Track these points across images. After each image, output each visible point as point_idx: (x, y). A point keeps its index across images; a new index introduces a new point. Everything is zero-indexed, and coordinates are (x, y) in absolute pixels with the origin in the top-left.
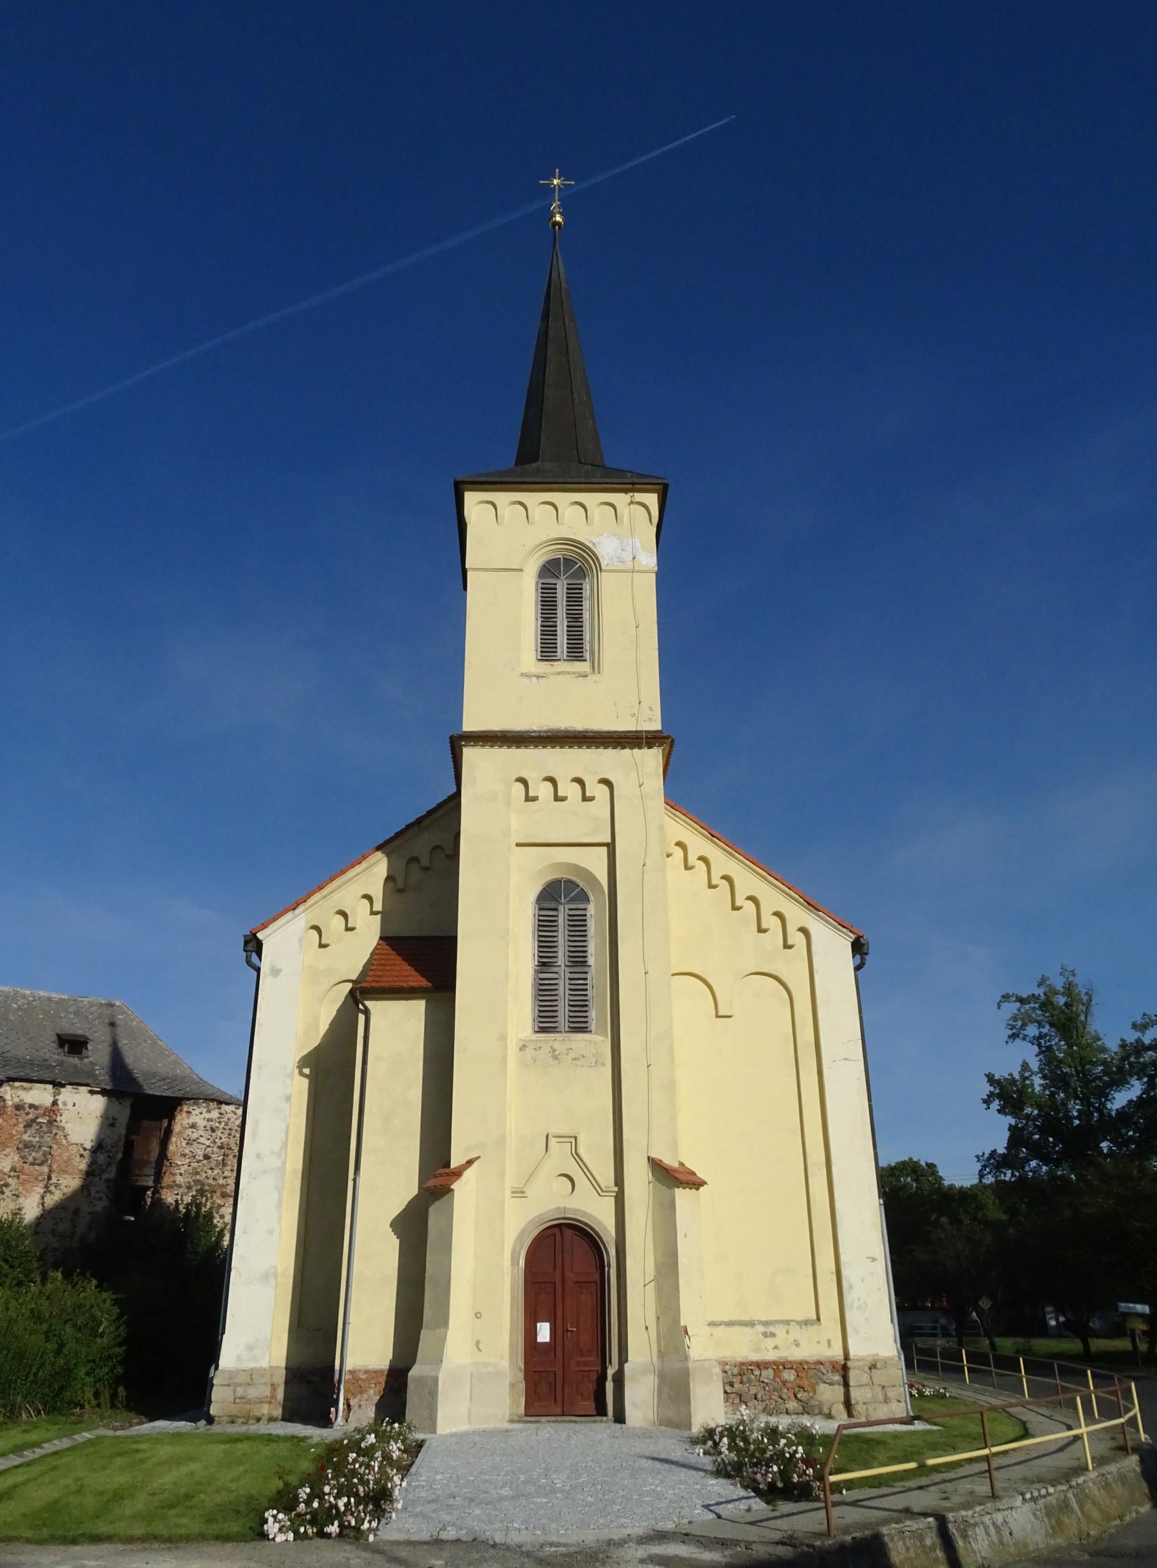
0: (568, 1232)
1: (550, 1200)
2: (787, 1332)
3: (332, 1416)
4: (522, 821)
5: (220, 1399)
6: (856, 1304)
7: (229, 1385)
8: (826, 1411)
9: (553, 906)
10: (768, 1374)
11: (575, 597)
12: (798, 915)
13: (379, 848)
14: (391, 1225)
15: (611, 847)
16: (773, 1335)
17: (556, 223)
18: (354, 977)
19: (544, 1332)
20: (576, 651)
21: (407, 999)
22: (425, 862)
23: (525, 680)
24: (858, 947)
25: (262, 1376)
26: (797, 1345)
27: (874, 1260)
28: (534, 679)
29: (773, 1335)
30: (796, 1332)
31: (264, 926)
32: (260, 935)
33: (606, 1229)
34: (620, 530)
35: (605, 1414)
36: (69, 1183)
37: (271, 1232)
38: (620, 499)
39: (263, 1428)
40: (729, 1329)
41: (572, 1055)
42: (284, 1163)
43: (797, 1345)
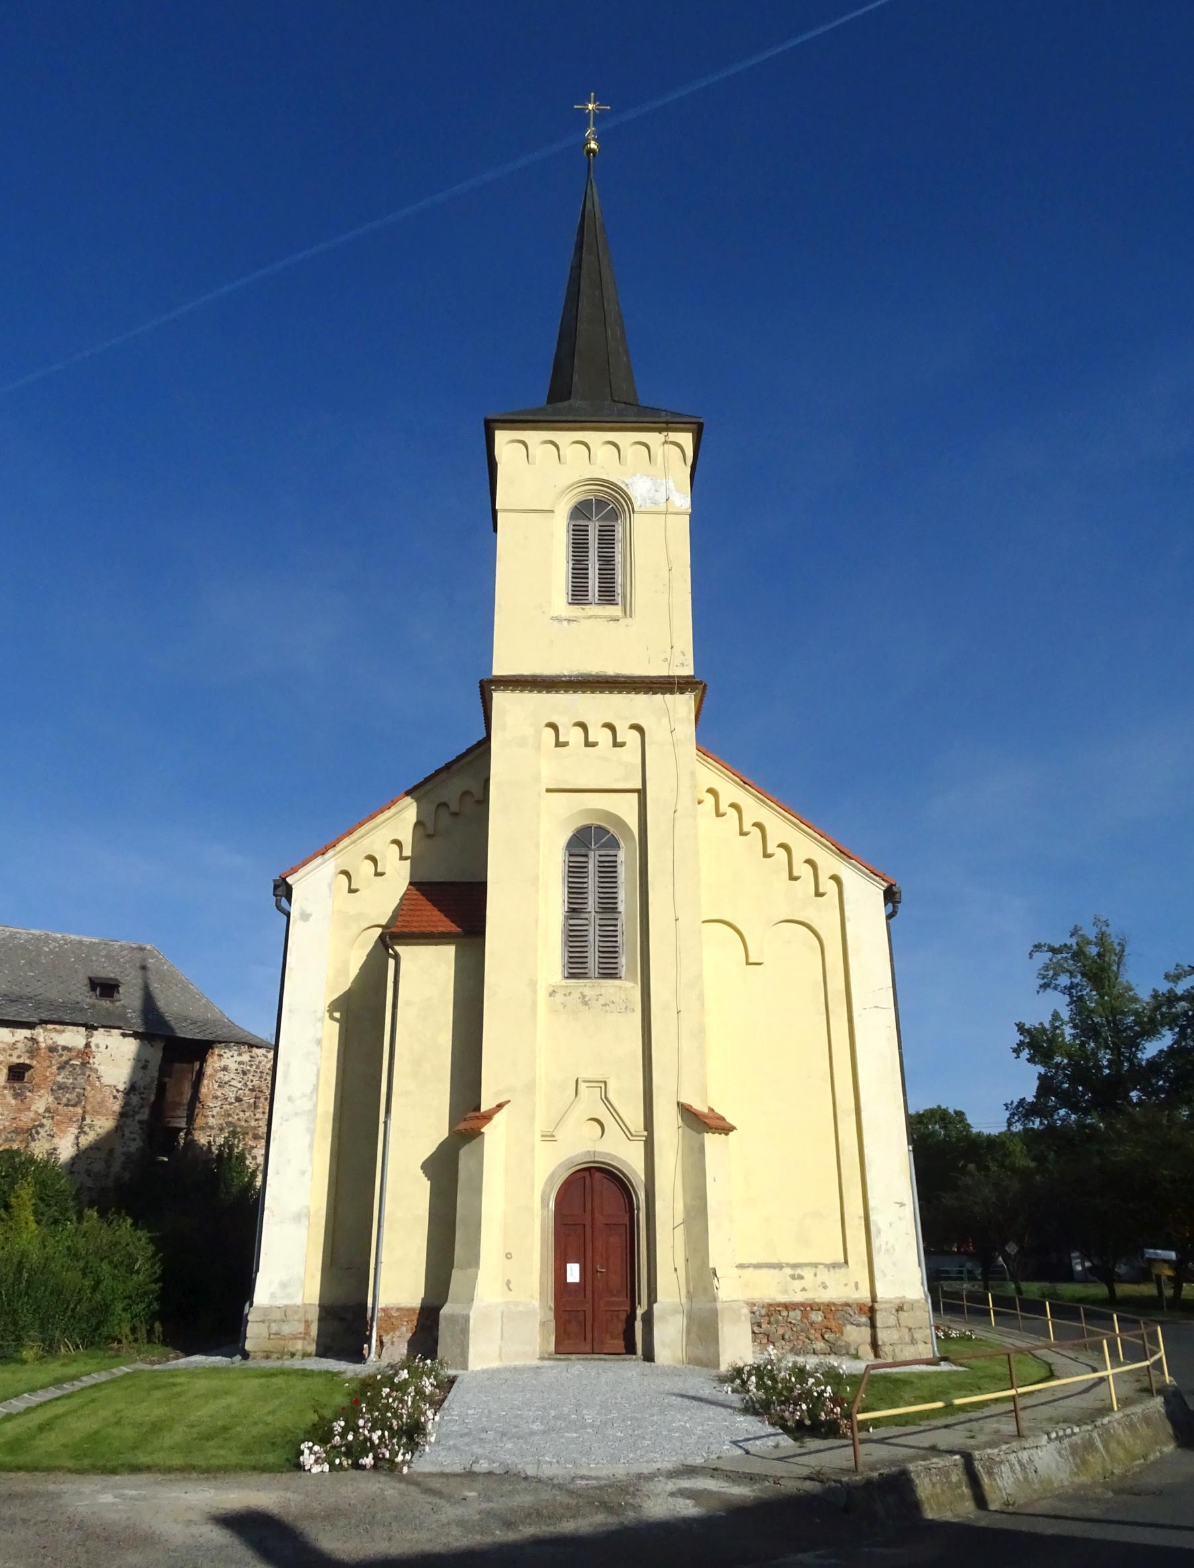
0: (598, 1175)
1: (579, 1143)
2: (815, 1275)
3: (365, 1352)
4: (555, 768)
5: (255, 1334)
6: (884, 1247)
7: (263, 1321)
8: (853, 1351)
9: (583, 852)
10: (795, 1316)
11: (607, 539)
12: (829, 862)
13: (408, 793)
14: (422, 1167)
15: (642, 793)
16: (801, 1277)
17: (591, 151)
18: (384, 923)
19: (573, 1273)
20: (608, 595)
21: (437, 944)
22: (454, 807)
23: (556, 623)
24: (890, 895)
25: (296, 1312)
26: (825, 1287)
27: (902, 1205)
28: (565, 623)
29: (801, 1277)
30: (824, 1275)
31: (294, 871)
32: (289, 880)
33: (635, 1172)
34: (654, 472)
35: (634, 1353)
36: (103, 1124)
37: (303, 1173)
38: (653, 438)
39: (298, 1363)
41: (602, 1001)
42: (315, 1105)
43: (825, 1287)
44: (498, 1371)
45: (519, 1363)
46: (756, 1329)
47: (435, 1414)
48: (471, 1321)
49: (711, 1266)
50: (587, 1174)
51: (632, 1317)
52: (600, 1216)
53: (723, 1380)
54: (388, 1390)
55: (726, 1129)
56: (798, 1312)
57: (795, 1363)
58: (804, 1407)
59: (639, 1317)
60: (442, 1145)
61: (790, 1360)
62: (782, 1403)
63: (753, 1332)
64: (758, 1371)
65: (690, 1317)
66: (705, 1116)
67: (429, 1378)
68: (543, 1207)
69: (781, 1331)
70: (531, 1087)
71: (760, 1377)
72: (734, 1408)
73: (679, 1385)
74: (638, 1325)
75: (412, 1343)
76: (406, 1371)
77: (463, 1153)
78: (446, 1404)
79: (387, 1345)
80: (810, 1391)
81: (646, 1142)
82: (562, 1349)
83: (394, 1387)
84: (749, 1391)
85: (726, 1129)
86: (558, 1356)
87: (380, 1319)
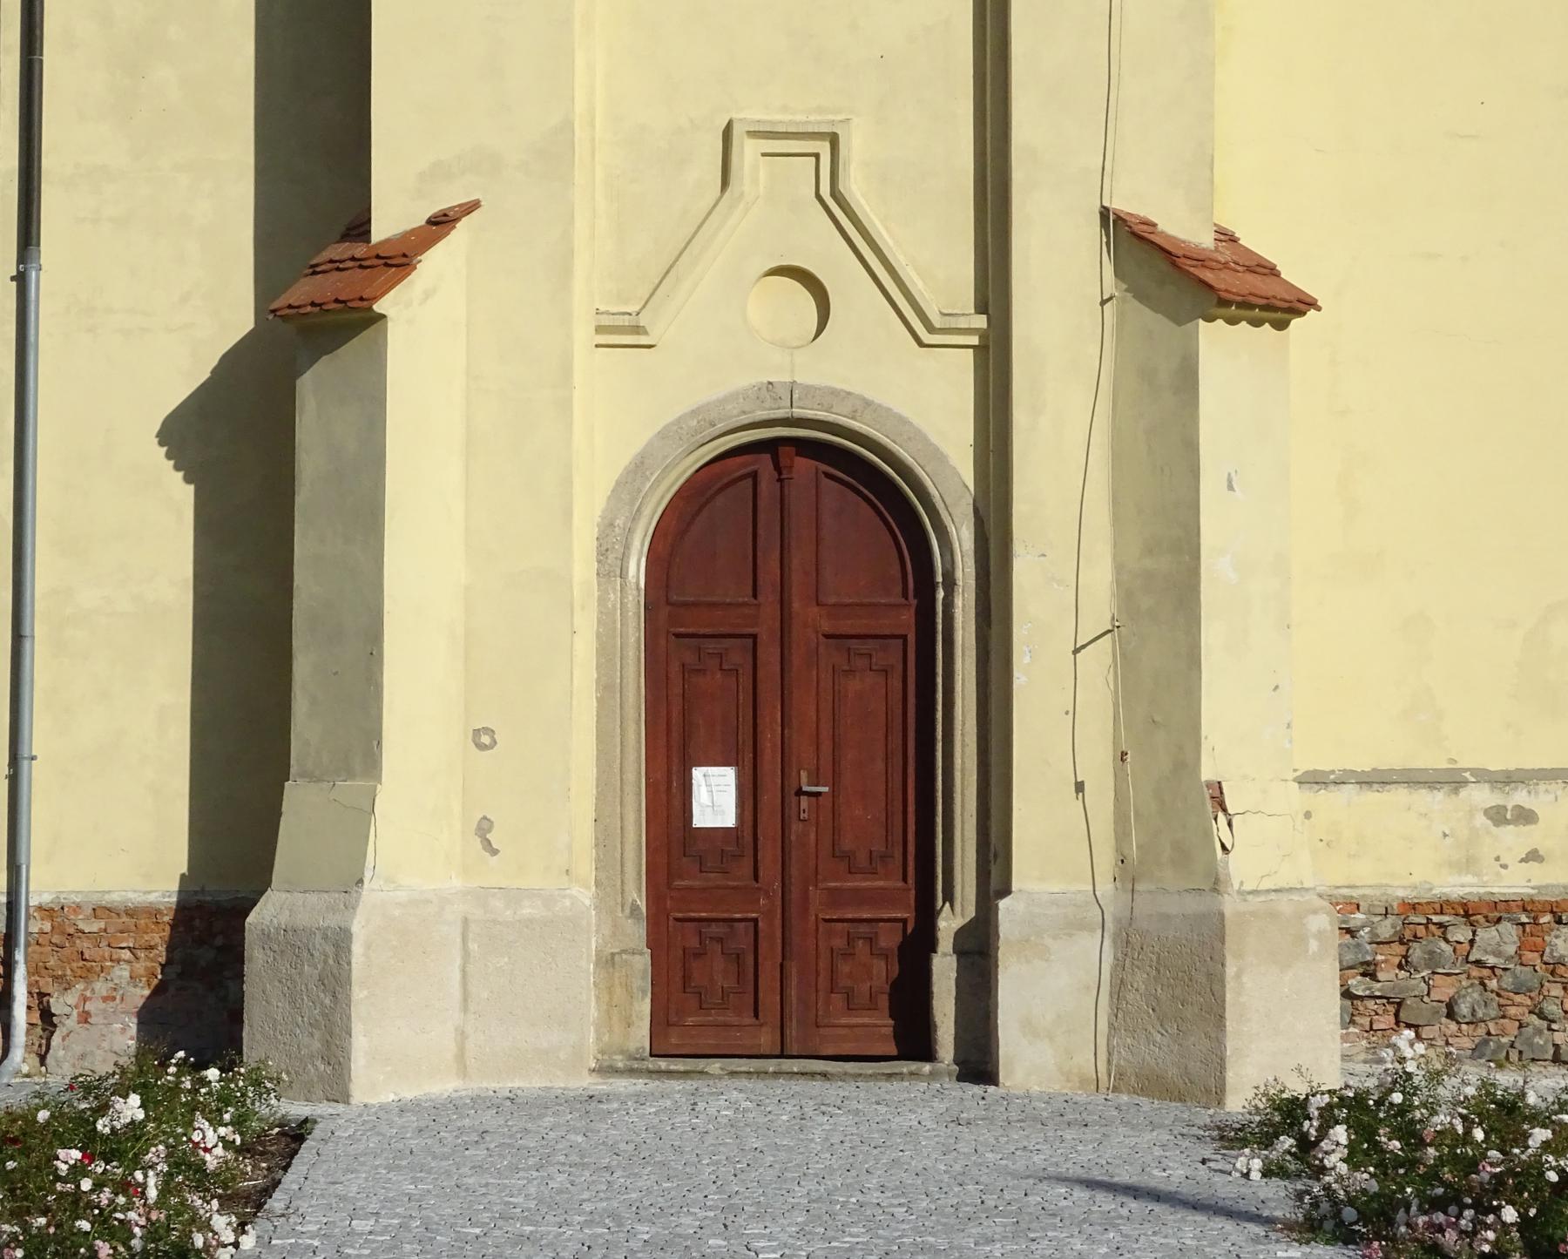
0: (804, 467)
1: (736, 357)
10: (1499, 940)
16: (1525, 817)
19: (715, 797)
29: (1525, 817)
33: (939, 457)
35: (926, 1052)
40: (1372, 797)
44: (454, 1105)
45: (529, 1083)
46: (1358, 985)
47: (241, 1229)
48: (357, 949)
49: (1207, 774)
50: (764, 463)
51: (921, 941)
52: (817, 640)
53: (1232, 1137)
54: (76, 1154)
55: (1281, 307)
56: (1509, 931)
57: (1486, 1086)
58: (1510, 1214)
59: (945, 942)
60: (234, 363)
61: (1468, 1080)
62: (1438, 1204)
63: (1347, 994)
64: (1356, 1109)
65: (1130, 943)
66: (1202, 260)
67: (216, 1122)
68: (603, 575)
69: (1444, 990)
70: (555, 154)
71: (1364, 1131)
72: (1269, 1221)
73: (1084, 1156)
74: (944, 969)
75: (151, 1018)
76: (135, 1099)
77: (315, 392)
78: (276, 1202)
79: (68, 1023)
80: (1534, 1169)
81: (981, 351)
82: (674, 1040)
83: (93, 1146)
84: (1323, 1170)
85: (1281, 307)
86: (663, 1064)
87: (36, 941)
